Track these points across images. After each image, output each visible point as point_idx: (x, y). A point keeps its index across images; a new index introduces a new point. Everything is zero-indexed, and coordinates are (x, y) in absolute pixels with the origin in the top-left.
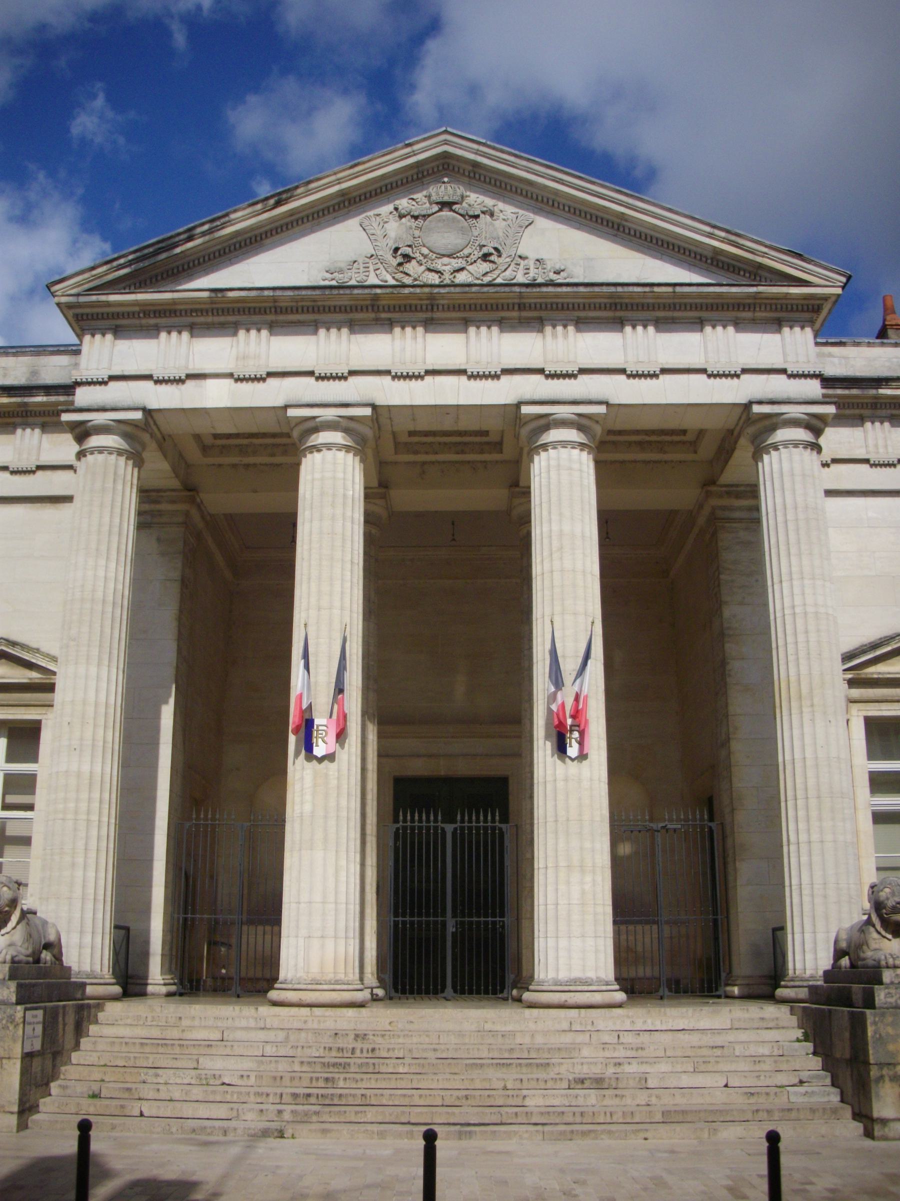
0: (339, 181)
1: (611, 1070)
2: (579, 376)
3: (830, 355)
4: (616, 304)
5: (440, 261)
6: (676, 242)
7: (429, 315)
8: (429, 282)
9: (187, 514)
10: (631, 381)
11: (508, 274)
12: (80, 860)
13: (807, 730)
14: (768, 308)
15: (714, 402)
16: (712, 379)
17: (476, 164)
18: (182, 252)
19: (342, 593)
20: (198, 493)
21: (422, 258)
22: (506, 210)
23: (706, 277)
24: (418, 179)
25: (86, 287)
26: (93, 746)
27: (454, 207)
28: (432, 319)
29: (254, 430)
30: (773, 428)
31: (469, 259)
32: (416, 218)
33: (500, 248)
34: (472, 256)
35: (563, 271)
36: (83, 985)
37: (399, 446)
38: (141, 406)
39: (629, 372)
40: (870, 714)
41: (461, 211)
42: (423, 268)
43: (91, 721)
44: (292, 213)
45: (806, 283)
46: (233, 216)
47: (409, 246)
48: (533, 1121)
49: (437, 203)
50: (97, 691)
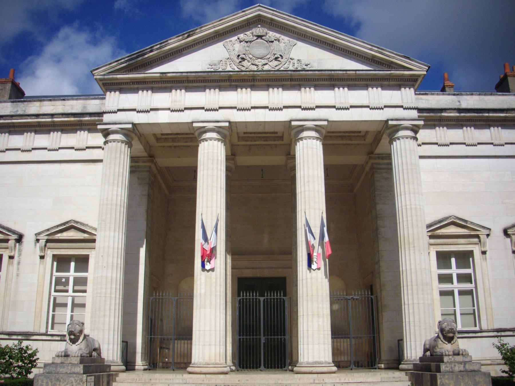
3: (421, 99)
4: (331, 79)
6: (357, 52)
7: (252, 83)
9: (150, 167)
13: (412, 257)
15: (373, 119)
17: (272, 20)
22: (285, 39)
25: (108, 71)
30: (397, 131)
32: (247, 42)
40: (438, 250)
41: (266, 39)
42: (250, 63)
43: (111, 255)
45: (411, 70)
46: (169, 42)
47: (244, 54)
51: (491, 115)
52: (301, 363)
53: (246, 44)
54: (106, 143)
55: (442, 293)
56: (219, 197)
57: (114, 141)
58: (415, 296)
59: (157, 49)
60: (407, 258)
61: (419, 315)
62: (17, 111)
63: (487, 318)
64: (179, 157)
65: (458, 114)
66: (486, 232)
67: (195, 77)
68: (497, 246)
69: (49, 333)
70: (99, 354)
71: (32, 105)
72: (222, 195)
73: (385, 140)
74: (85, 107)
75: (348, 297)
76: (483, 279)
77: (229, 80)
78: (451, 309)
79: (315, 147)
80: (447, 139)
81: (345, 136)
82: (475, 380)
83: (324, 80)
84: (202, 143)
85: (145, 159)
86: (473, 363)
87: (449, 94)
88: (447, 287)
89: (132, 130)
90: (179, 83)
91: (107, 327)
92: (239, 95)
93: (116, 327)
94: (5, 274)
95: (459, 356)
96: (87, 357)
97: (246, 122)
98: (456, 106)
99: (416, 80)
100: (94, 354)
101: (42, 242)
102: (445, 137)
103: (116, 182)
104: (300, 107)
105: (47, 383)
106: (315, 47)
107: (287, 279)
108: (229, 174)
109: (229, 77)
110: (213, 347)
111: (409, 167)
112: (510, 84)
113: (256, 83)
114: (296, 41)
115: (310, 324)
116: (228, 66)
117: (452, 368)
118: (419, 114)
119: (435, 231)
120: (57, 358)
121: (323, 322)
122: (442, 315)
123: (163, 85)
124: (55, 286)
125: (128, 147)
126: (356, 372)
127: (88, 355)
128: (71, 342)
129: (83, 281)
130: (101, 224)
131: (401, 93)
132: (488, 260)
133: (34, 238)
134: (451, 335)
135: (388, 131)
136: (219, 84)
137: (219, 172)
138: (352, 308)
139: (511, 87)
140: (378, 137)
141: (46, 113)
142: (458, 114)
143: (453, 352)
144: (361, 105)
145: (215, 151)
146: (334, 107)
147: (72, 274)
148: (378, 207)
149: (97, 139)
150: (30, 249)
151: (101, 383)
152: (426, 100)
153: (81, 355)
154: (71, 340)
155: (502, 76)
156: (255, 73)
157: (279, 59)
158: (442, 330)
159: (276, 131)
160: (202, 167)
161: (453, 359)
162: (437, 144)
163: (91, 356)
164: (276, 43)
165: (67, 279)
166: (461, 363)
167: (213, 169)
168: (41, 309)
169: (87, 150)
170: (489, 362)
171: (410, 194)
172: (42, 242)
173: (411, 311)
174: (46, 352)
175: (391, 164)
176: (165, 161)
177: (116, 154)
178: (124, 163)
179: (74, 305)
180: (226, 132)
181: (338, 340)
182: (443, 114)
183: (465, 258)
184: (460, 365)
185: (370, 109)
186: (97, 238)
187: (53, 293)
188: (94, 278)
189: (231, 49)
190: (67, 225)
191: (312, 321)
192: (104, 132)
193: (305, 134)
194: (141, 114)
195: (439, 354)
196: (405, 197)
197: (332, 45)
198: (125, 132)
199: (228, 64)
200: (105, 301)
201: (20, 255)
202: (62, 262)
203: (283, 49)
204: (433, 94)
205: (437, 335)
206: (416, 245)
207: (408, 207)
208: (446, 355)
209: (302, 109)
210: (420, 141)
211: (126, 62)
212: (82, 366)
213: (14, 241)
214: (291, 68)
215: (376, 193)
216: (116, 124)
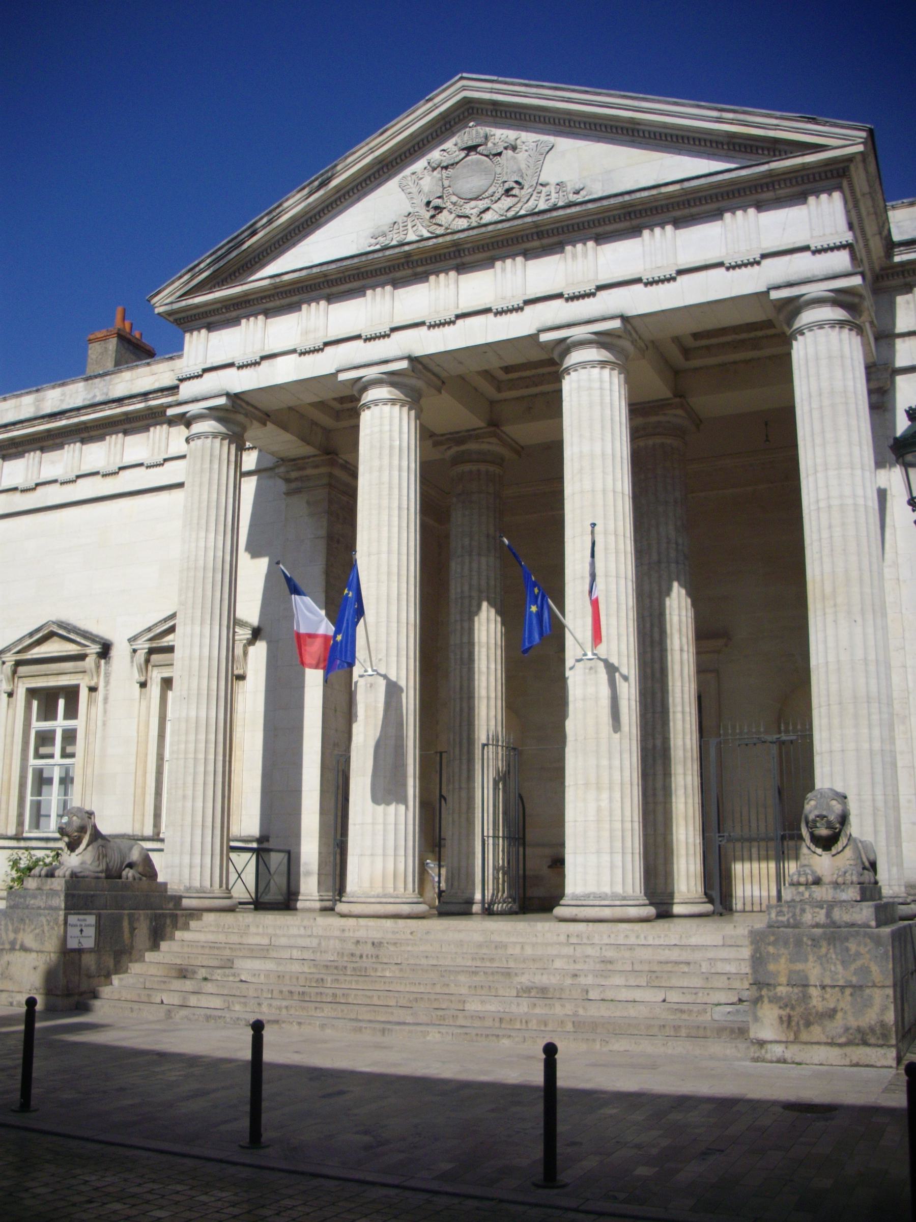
0: (372, 151)
1: (569, 981)
2: (598, 294)
4: (629, 213)
5: (468, 206)
6: (690, 134)
7: (459, 261)
8: (460, 228)
9: (330, 475)
10: (649, 288)
11: (531, 204)
12: (190, 793)
13: (830, 631)
14: (794, 182)
15: (733, 295)
16: (731, 270)
17: (495, 103)
18: (249, 247)
19: (389, 538)
20: (337, 455)
21: (451, 206)
22: (528, 138)
23: (728, 162)
24: (447, 130)
25: (178, 294)
26: (198, 694)
27: (479, 149)
28: (463, 264)
30: (797, 312)
31: (493, 198)
32: (446, 168)
33: (520, 180)
34: (496, 194)
35: (582, 189)
36: (180, 898)
37: (687, 352)
38: (224, 392)
39: (645, 281)
41: (485, 152)
42: (453, 216)
43: (196, 674)
44: (338, 188)
46: (285, 205)
47: (439, 197)
48: (458, 1024)
49: (463, 149)
50: (201, 646)
62: (95, 396)
71: (119, 380)
77: (408, 262)
81: (743, 341)
82: (847, 949)
89: (231, 408)
94: (84, 723)
101: (141, 656)
103: (203, 521)
105: (6, 925)
106: (599, 141)
114: (551, 139)
117: (794, 915)
121: (611, 800)
131: (809, 213)
136: (391, 275)
147: (60, 724)
161: (807, 895)
177: (202, 464)
184: (817, 910)
201: (107, 683)
209: (567, 300)
211: (209, 266)
213: (94, 656)
214: (542, 206)
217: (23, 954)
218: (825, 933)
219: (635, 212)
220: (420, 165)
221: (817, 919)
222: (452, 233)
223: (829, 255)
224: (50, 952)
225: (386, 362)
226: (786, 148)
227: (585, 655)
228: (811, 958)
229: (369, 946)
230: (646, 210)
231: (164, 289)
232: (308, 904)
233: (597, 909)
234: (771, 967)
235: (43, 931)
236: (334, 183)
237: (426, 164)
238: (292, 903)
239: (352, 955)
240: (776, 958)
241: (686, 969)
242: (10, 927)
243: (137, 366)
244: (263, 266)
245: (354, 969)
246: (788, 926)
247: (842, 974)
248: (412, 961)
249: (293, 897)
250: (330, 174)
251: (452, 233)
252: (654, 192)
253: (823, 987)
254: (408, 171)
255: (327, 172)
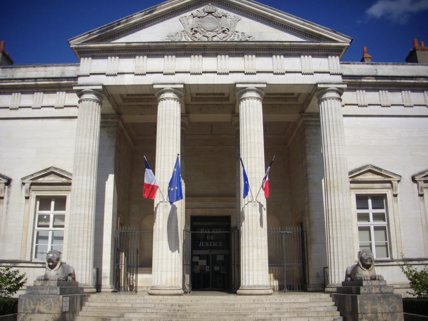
0: (172, 4)
5: (207, 33)
6: (291, 27)
7: (204, 52)
9: (117, 123)
11: (232, 37)
12: (81, 245)
15: (304, 83)
22: (231, 14)
28: (205, 54)
29: (142, 93)
30: (325, 93)
32: (199, 17)
41: (215, 15)
42: (202, 35)
44: (156, 15)
46: (134, 17)
47: (197, 28)
51: (403, 81)
52: (243, 287)
53: (198, 19)
54: (80, 101)
55: (361, 229)
56: (175, 147)
57: (87, 100)
58: (339, 231)
59: (124, 23)
60: (332, 199)
61: (342, 247)
62: (7, 76)
63: (397, 249)
64: (142, 115)
65: (375, 81)
66: (397, 178)
67: (155, 46)
68: (406, 190)
69: (33, 261)
70: (74, 279)
71: (18, 71)
72: (178, 146)
73: (314, 100)
74: (63, 73)
75: (282, 232)
76: (394, 217)
78: (367, 242)
79: (256, 106)
80: (365, 101)
81: (281, 98)
82: (389, 301)
83: (264, 50)
84: (161, 102)
85: (113, 116)
86: (387, 287)
87: (368, 64)
88: (364, 224)
90: (142, 51)
91: (80, 256)
92: (193, 62)
93: (89, 256)
95: (376, 281)
96: (63, 280)
97: (198, 84)
98: (374, 73)
99: (341, 51)
100: (70, 278)
101: (27, 185)
102: (364, 100)
103: (88, 134)
104: (243, 72)
105: (29, 302)
107: (231, 217)
108: (184, 129)
109: (184, 47)
110: (169, 273)
111: (335, 124)
112: (418, 57)
113: (207, 52)
114: (240, 16)
115: (251, 253)
116: (184, 38)
117: (369, 290)
118: (343, 80)
119: (355, 177)
120: (37, 281)
122: (360, 246)
123: (128, 53)
124: (39, 221)
125: (99, 105)
126: (289, 295)
127: (64, 279)
128: (50, 268)
129: (62, 218)
130: (76, 169)
132: (398, 202)
133: (20, 182)
134: (369, 263)
135: (317, 93)
137: (175, 126)
138: (286, 241)
139: (419, 59)
140: (308, 99)
141: (30, 77)
142: (375, 81)
143: (371, 277)
144: (295, 71)
145: (172, 109)
146: (272, 72)
147: (52, 212)
148: (308, 157)
149: (73, 98)
150: (17, 191)
151: (75, 303)
152: (348, 68)
153: (58, 279)
154: (49, 266)
155: (411, 50)
156: (206, 43)
157: (226, 32)
158: (361, 259)
159: (223, 92)
160: (161, 122)
161: (370, 283)
162: (357, 105)
163: (67, 280)
164: (224, 18)
165: (48, 216)
166: (376, 286)
167: (170, 124)
168: (27, 241)
169: (65, 108)
170: (398, 286)
171: (335, 145)
172: (27, 185)
173: (335, 243)
174: (31, 276)
175: (319, 121)
176: (130, 118)
178: (95, 118)
179: (55, 238)
180: (182, 93)
181: (274, 268)
182: (363, 80)
183: (379, 200)
185: (302, 74)
186: (73, 182)
187: (36, 228)
188: (70, 215)
189: (186, 23)
190: (48, 171)
191: (253, 252)
192: (79, 93)
193: (248, 94)
194: (109, 77)
195: (358, 279)
196: (331, 148)
197: (271, 21)
198: (96, 92)
199: (183, 36)
200: (79, 234)
201: (9, 196)
202: (44, 202)
203: (229, 24)
204: (355, 64)
205: (357, 263)
206: (339, 188)
207: (333, 156)
208: (365, 280)
209: (245, 74)
210: (343, 102)
211: (98, 33)
212: (58, 288)
213: (3, 185)
214: (236, 39)
215: (306, 145)
216: (88, 85)
217: (40, 315)
218: (382, 296)
219: (272, 49)
220: (188, 14)
221: (377, 291)
222: (201, 42)
223: (335, 76)
224: (55, 314)
225: (174, 84)
226: (324, 39)
227: (164, 200)
228: (378, 304)
229: (177, 306)
230: (276, 49)
231: (76, 38)
232: (106, 290)
233: (260, 290)
234: (366, 307)
235: (51, 305)
236: (155, 13)
237: (190, 14)
238: (99, 290)
239: (174, 310)
240: (367, 304)
241: (306, 310)
242: (32, 303)
243: (29, 66)
244: (119, 38)
245: (180, 316)
246: (367, 294)
247: (388, 309)
248: (200, 312)
249: (99, 287)
250: (154, 9)
251: (201, 42)
252: (281, 43)
253: (382, 313)
254: (183, 15)
255: (153, 8)
